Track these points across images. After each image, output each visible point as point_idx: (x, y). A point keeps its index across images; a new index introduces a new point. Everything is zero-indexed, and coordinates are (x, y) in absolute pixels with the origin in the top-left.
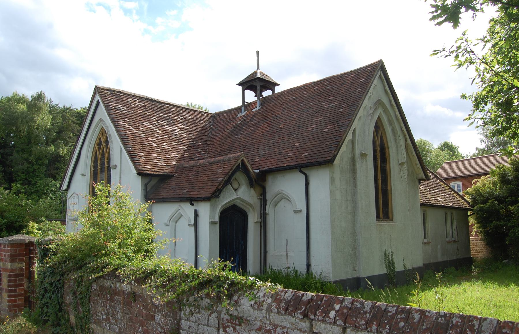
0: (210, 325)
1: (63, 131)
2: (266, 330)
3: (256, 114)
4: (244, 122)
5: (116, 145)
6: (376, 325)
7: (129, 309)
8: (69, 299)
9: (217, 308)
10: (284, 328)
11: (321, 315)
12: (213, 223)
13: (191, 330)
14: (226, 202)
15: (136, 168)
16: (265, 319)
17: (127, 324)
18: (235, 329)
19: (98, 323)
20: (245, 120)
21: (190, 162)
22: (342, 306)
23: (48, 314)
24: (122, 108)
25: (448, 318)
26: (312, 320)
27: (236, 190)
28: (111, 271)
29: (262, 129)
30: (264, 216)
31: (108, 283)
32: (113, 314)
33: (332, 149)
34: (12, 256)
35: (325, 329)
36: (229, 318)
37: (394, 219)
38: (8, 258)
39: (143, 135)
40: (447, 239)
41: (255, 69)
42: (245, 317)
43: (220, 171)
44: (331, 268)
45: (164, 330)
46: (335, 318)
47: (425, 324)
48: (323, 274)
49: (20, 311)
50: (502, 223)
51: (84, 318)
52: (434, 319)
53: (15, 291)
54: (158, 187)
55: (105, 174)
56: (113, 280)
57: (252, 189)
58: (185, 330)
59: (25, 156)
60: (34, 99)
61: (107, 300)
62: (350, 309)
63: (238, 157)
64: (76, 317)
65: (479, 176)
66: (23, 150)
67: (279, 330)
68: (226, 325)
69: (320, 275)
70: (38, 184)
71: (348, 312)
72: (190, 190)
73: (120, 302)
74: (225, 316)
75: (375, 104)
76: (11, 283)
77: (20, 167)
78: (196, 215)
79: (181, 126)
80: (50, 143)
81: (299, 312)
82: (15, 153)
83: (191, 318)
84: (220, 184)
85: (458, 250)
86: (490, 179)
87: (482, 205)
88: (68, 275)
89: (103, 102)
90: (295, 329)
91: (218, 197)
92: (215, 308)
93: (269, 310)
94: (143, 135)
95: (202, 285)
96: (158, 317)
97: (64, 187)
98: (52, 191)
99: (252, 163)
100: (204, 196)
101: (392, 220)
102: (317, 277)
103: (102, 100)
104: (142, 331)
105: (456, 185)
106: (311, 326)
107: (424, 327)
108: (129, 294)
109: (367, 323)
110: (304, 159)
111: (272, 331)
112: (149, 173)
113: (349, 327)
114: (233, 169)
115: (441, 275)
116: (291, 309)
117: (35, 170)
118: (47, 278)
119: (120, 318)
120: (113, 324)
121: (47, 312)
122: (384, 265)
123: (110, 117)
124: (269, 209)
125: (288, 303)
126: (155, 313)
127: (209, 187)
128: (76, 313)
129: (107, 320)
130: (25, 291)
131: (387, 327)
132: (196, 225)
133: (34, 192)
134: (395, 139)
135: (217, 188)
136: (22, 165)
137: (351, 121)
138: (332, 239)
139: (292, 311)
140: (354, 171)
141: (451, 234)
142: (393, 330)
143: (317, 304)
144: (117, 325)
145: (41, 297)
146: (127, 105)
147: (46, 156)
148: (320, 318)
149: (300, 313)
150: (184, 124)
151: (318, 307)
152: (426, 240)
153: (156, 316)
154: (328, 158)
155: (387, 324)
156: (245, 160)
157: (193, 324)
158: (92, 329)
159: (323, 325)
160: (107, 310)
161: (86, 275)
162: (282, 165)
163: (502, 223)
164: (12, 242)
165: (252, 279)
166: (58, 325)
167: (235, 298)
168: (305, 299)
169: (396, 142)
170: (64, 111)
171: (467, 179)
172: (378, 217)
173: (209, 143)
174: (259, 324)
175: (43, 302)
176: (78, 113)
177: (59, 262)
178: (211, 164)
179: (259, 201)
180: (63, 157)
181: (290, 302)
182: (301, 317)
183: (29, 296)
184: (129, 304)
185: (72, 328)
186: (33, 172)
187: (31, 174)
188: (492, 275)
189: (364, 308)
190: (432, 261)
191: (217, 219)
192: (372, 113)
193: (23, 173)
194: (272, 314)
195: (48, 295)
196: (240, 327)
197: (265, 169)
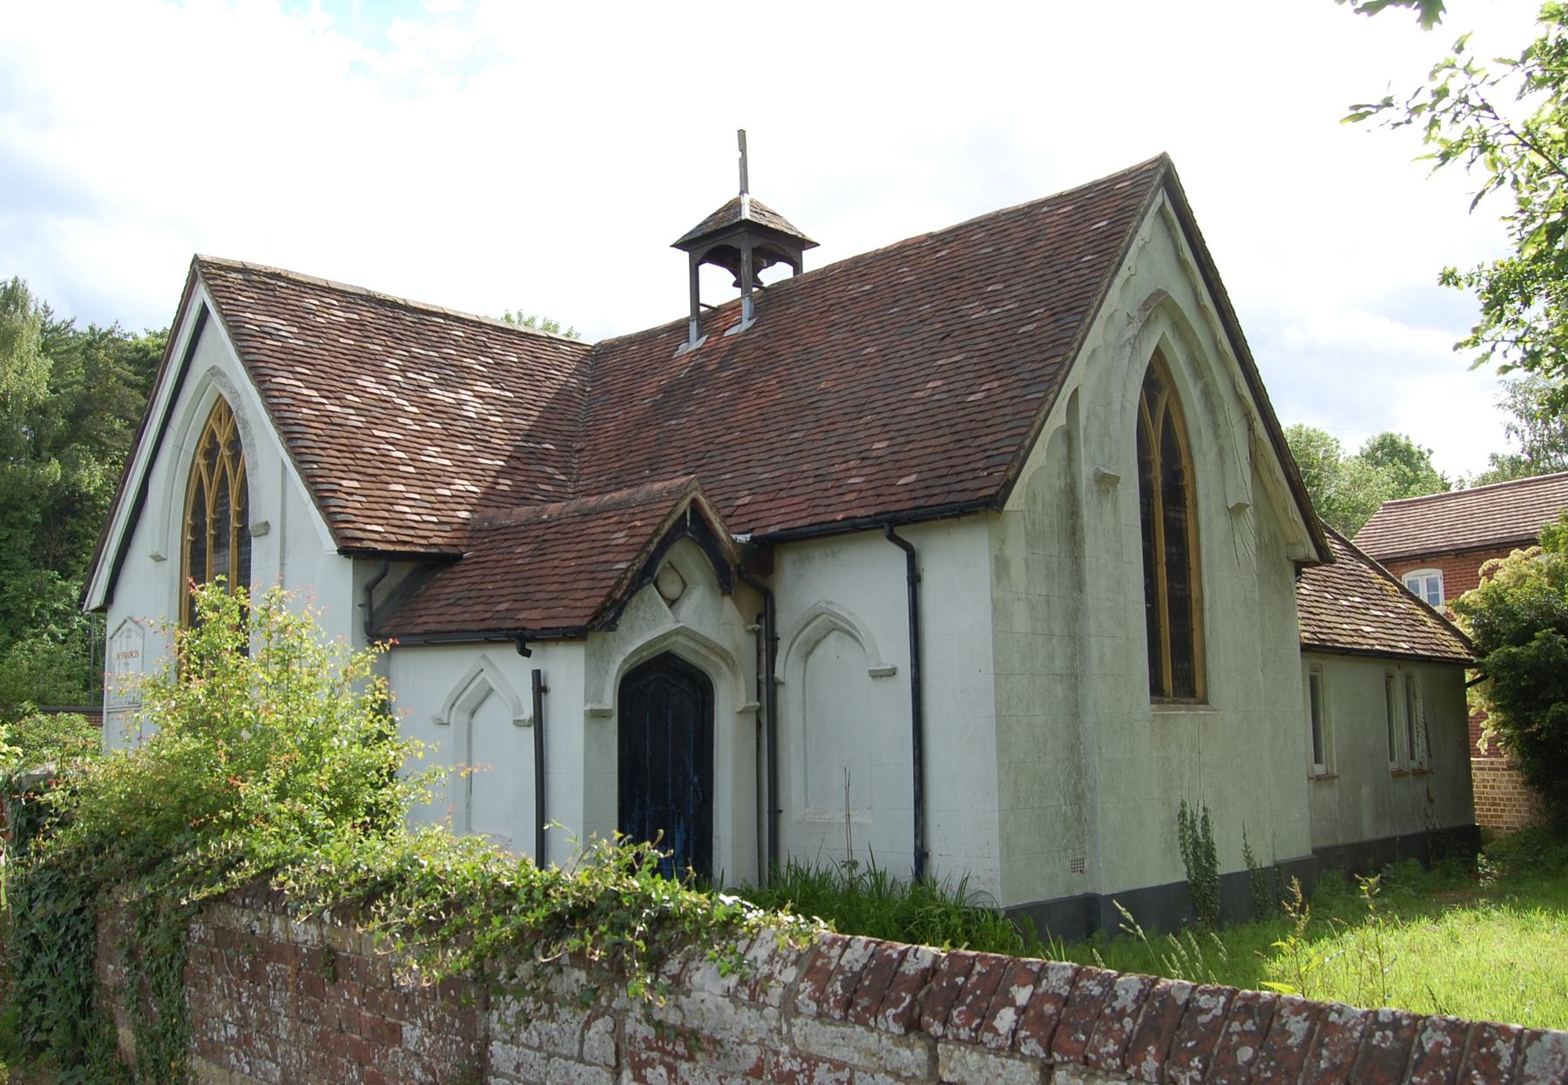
0: (587, 1058)
1: (90, 412)
2: (780, 1073)
3: (736, 345)
5: (267, 455)
6: (1156, 1057)
7: (315, 1006)
8: (113, 972)
9: (610, 1000)
10: (838, 1066)
11: (967, 1023)
12: (596, 716)
14: (639, 643)
15: (336, 532)
16: (776, 1037)
17: (308, 1056)
18: (672, 1070)
19: (212, 1051)
20: (701, 366)
21: (517, 510)
22: (1040, 991)
23: (45, 1025)
24: (286, 330)
25: (1405, 1034)
26: (936, 1040)
27: (672, 603)
30: (768, 690)
31: (242, 920)
32: (262, 1023)
33: (997, 460)
35: (980, 1070)
37: (1211, 698)
39: (355, 420)
40: (1393, 766)
42: (706, 1032)
43: (620, 537)
44: (997, 863)
45: (434, 1075)
46: (1014, 1032)
47: (1325, 1052)
51: (164, 1034)
52: (1357, 1034)
54: (410, 594)
56: (260, 909)
57: (727, 601)
61: (243, 975)
62: (1066, 1001)
64: (138, 1032)
65: (1501, 548)
68: (644, 1056)
69: (962, 889)
71: (1058, 1013)
72: (517, 605)
73: (285, 982)
74: (640, 1028)
75: (1145, 306)
78: (540, 689)
79: (484, 387)
80: (45, 454)
81: (891, 1012)
83: (524, 1035)
84: (618, 585)
85: (1431, 801)
87: (1514, 650)
90: (877, 1071)
91: (611, 626)
93: (789, 1008)
94: (355, 420)
95: (562, 923)
96: (412, 1033)
97: (96, 599)
99: (727, 511)
100: (566, 623)
101: (1204, 701)
103: (218, 304)
105: (1423, 579)
106: (934, 1059)
107: (1323, 1064)
108: (312, 955)
110: (905, 496)
113: (1063, 1063)
114: (663, 532)
116: (864, 1002)
118: (38, 904)
119: (284, 1036)
120: (261, 1055)
121: (40, 1019)
122: (1178, 852)
126: (402, 1018)
127: (584, 594)
128: (140, 1020)
129: (243, 1042)
131: (1196, 1062)
132: (539, 722)
134: (1215, 426)
135: (609, 596)
137: (1062, 364)
138: (1000, 766)
140: (1073, 535)
141: (1406, 747)
142: (1216, 1073)
144: (274, 1060)
145: (21, 967)
147: (34, 497)
148: (964, 1033)
149: (895, 1018)
150: (494, 383)
151: (958, 995)
152: (1320, 769)
153: (407, 1029)
156: (702, 500)
157: (531, 1053)
159: (973, 1058)
160: (241, 1009)
162: (828, 518)
166: (81, 1059)
167: (673, 966)
168: (910, 968)
169: (1217, 436)
171: (1461, 560)
172: (1156, 690)
173: (579, 446)
174: (754, 1053)
175: (27, 982)
176: (138, 350)
178: (587, 515)
179: (752, 639)
181: (861, 980)
182: (897, 1029)
184: (313, 988)
189: (1116, 997)
190: (1341, 841)
191: (610, 701)
194: (799, 1021)
195: (42, 960)
197: (771, 530)
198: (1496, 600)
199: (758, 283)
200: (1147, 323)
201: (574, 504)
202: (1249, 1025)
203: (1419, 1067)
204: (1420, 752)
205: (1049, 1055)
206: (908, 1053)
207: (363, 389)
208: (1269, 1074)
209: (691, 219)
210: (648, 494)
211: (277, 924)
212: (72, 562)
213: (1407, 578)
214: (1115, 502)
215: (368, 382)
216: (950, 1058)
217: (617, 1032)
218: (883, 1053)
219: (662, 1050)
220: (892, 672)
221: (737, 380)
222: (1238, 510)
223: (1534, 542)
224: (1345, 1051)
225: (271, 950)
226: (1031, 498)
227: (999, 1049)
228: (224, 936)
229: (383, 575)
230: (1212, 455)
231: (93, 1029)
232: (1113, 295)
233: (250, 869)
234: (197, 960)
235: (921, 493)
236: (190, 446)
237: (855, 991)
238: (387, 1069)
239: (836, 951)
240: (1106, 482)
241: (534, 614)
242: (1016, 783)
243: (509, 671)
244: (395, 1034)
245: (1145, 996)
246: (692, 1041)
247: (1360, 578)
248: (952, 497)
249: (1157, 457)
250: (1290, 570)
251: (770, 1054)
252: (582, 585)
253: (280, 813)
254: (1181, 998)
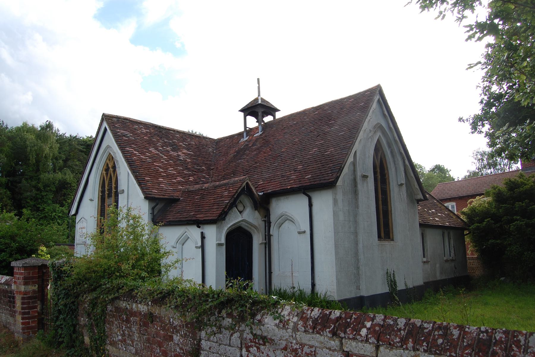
0: (232, 345)
1: (70, 159)
2: (293, 349)
3: (257, 139)
4: (247, 147)
5: (124, 172)
6: (412, 342)
7: (146, 330)
8: (83, 320)
9: (239, 327)
10: (311, 347)
11: (352, 333)
12: (219, 245)
13: (212, 350)
14: (232, 224)
15: (144, 192)
16: (291, 338)
17: (144, 345)
18: (258, 348)
19: (113, 344)
20: (247, 145)
21: (195, 186)
22: (374, 323)
23: (63, 336)
24: (129, 134)
25: (490, 334)
26: (342, 338)
27: (241, 212)
28: (127, 292)
29: (265, 153)
30: (268, 237)
31: (123, 304)
32: (129, 335)
33: (334, 171)
34: (25, 278)
35: (356, 347)
36: (252, 337)
38: (21, 281)
39: (149, 160)
40: (445, 258)
41: (257, 96)
42: (269, 337)
43: (226, 193)
44: (335, 287)
45: (183, 350)
46: (367, 336)
47: (465, 340)
48: (328, 294)
49: (34, 333)
50: (498, 241)
51: (99, 339)
52: (475, 335)
53: (28, 313)
54: (166, 210)
55: (113, 198)
56: (129, 301)
57: (256, 212)
58: (205, 350)
59: (34, 183)
60: (42, 128)
61: (123, 321)
62: (382, 326)
63: (242, 181)
64: (91, 338)
65: (474, 196)
66: (31, 178)
67: (306, 349)
68: (249, 344)
69: (325, 295)
70: (46, 210)
71: (380, 330)
72: (196, 213)
73: (137, 323)
74: (248, 336)
75: (375, 127)
76: (25, 306)
77: (29, 194)
78: (203, 237)
79: (185, 151)
80: (57, 171)
81: (328, 330)
82: (24, 181)
83: (212, 338)
84: (226, 207)
85: (456, 268)
86: (485, 199)
87: (479, 225)
88: (83, 296)
89: (110, 129)
90: (324, 348)
91: (224, 219)
92: (237, 328)
93: (295, 329)
94: (149, 160)
95: (223, 305)
96: (176, 338)
97: (73, 212)
98: (59, 217)
99: (256, 186)
100: (211, 218)
101: (393, 240)
102: (322, 297)
103: (110, 127)
104: (160, 352)
105: (450, 205)
106: (341, 344)
107: (465, 344)
108: (145, 315)
109: (402, 340)
110: (308, 181)
111: (299, 350)
112: (156, 196)
113: (383, 345)
114: (238, 192)
115: (465, 291)
116: (319, 327)
117: (43, 196)
118: (60, 300)
119: (136, 339)
120: (129, 344)
121: (61, 334)
122: (386, 283)
123: (117, 144)
124: (273, 231)
125: (315, 321)
126: (173, 333)
127: (216, 210)
128: (91, 334)
129: (124, 341)
130: (38, 313)
131: (425, 344)
132: (203, 247)
133: (42, 218)
134: (394, 162)
135: (223, 210)
136: (30, 192)
137: (352, 143)
138: (336, 259)
139: (320, 329)
140: (355, 192)
141: (449, 253)
142: (431, 347)
143: (347, 322)
144: (133, 346)
145: (55, 319)
146: (133, 132)
147: (54, 183)
148: (351, 336)
149: (329, 332)
150: (188, 150)
151: (348, 325)
152: (425, 260)
153: (175, 336)
154: (331, 180)
155: (424, 341)
156: (249, 183)
157: (214, 344)
158: (108, 350)
159: (354, 344)
160: (123, 331)
161: (102, 297)
162: (286, 188)
163: (498, 241)
164: (25, 265)
165: (274, 297)
166: (73, 346)
167: (259, 317)
168: (333, 317)
169: (395, 164)
170: (70, 140)
171: (461, 199)
172: (379, 237)
173: (212, 168)
174: (284, 343)
175: (58, 323)
176: (84, 142)
177: (73, 284)
178: (216, 187)
179: (264, 223)
180: (70, 184)
181: (318, 321)
182: (330, 335)
183: (43, 318)
184: (146, 325)
185: (87, 349)
186: (41, 199)
187: (39, 200)
188: (490, 292)
189: (398, 325)
191: (223, 241)
192: (372, 136)
193: (31, 200)
194: (299, 333)
195: (61, 317)
196: (264, 347)
197: (269, 191)
198: (473, 210)
199: (263, 121)
200: (375, 132)
201: (212, 184)
202: (441, 332)
203: (495, 344)
204: (452, 254)
205: (378, 342)
206: (333, 342)
207: (151, 151)
208: (448, 347)
209: (244, 103)
210: (234, 181)
211: (134, 305)
212: (64, 202)
213: (446, 205)
214: (367, 183)
215: (152, 149)
216: (347, 344)
217: (241, 337)
218: (326, 343)
219: (255, 343)
220: (304, 232)
221: (258, 149)
222: (402, 185)
223: (483, 194)
224: (471, 340)
225: (133, 314)
226: (344, 182)
227: (362, 341)
228: (118, 309)
229: (157, 205)
230: (393, 169)
231: (77, 337)
232: (366, 124)
233: (126, 289)
234: (109, 316)
235: (312, 180)
236: (101, 168)
237: (316, 324)
238: (169, 348)
239: (309, 312)
240: (365, 177)
241: (201, 216)
243: (194, 232)
244: (171, 338)
245: (406, 324)
246: (265, 340)
247: (434, 204)
248: (322, 182)
249: (378, 170)
250: (416, 202)
251: (289, 343)
252: (215, 207)
253: (133, 273)
254: (419, 324)
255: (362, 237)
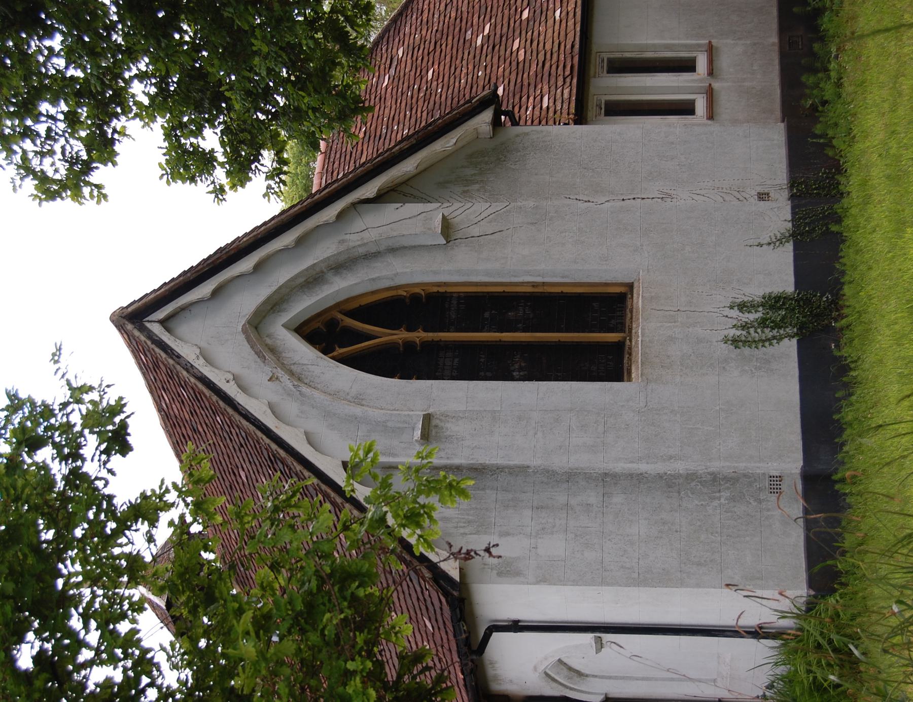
37: (627, 280)
101: (631, 286)
138: (681, 584)
190: (774, 39)
242: (699, 564)
255: (618, 458)
